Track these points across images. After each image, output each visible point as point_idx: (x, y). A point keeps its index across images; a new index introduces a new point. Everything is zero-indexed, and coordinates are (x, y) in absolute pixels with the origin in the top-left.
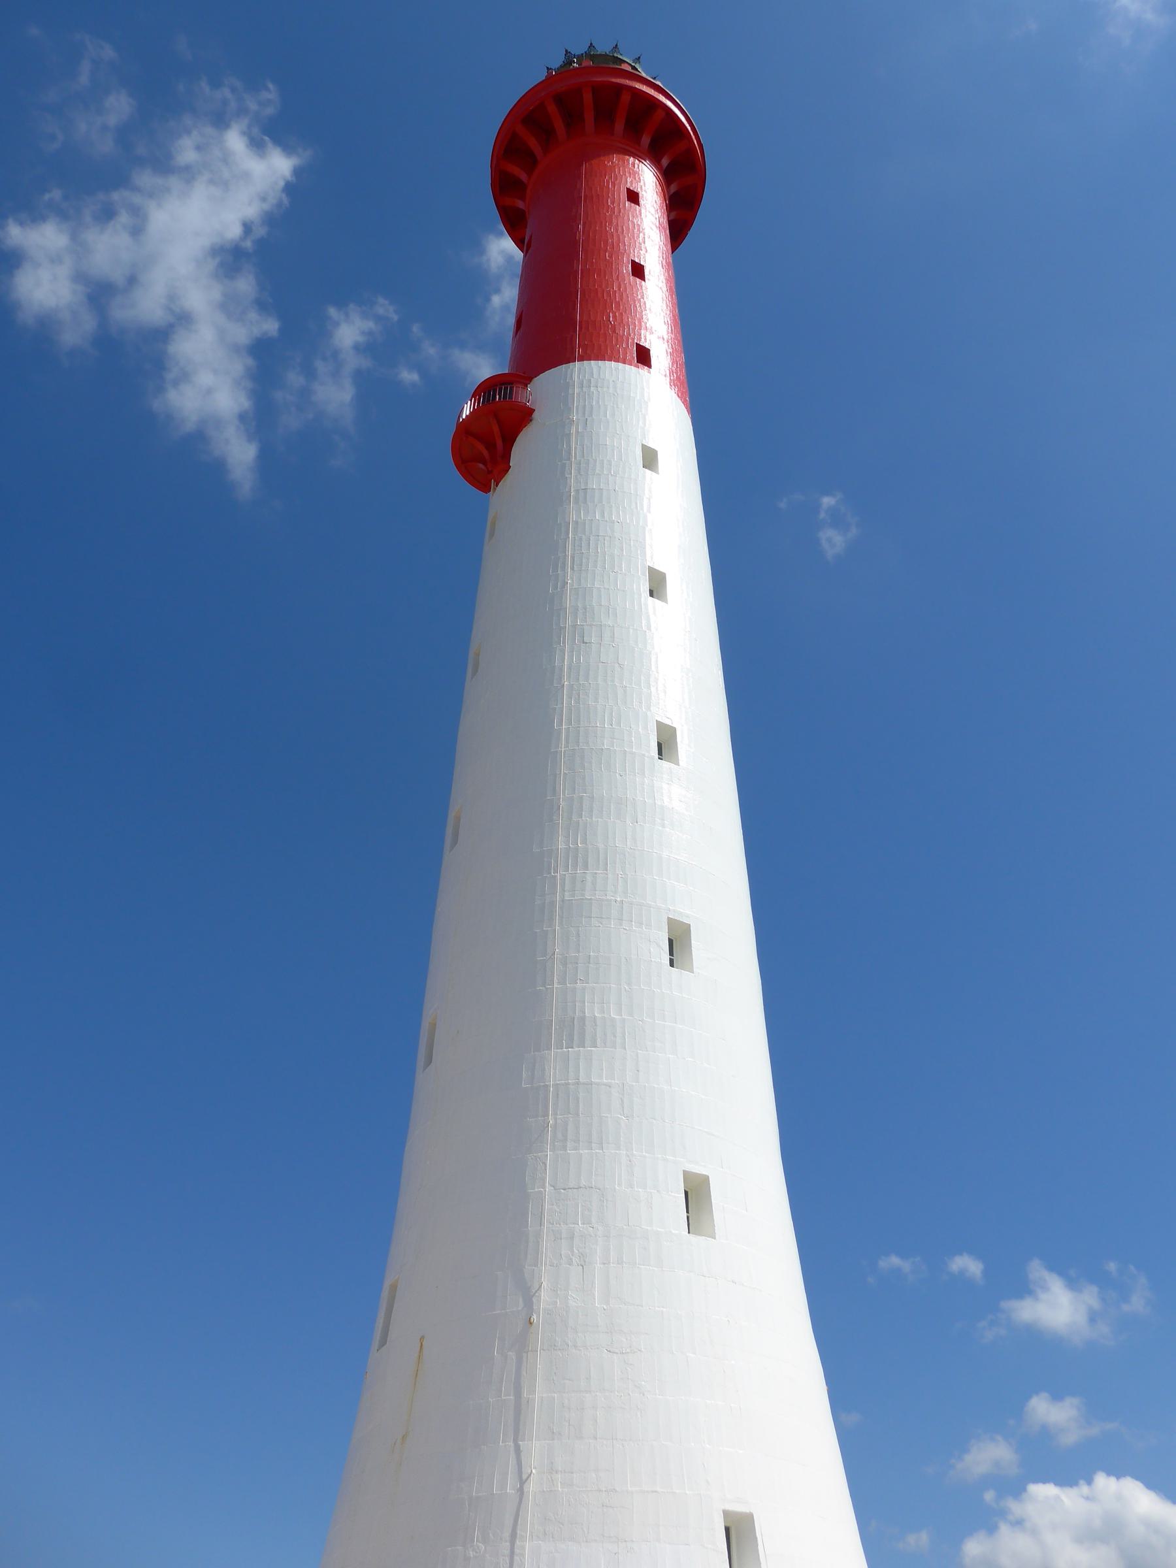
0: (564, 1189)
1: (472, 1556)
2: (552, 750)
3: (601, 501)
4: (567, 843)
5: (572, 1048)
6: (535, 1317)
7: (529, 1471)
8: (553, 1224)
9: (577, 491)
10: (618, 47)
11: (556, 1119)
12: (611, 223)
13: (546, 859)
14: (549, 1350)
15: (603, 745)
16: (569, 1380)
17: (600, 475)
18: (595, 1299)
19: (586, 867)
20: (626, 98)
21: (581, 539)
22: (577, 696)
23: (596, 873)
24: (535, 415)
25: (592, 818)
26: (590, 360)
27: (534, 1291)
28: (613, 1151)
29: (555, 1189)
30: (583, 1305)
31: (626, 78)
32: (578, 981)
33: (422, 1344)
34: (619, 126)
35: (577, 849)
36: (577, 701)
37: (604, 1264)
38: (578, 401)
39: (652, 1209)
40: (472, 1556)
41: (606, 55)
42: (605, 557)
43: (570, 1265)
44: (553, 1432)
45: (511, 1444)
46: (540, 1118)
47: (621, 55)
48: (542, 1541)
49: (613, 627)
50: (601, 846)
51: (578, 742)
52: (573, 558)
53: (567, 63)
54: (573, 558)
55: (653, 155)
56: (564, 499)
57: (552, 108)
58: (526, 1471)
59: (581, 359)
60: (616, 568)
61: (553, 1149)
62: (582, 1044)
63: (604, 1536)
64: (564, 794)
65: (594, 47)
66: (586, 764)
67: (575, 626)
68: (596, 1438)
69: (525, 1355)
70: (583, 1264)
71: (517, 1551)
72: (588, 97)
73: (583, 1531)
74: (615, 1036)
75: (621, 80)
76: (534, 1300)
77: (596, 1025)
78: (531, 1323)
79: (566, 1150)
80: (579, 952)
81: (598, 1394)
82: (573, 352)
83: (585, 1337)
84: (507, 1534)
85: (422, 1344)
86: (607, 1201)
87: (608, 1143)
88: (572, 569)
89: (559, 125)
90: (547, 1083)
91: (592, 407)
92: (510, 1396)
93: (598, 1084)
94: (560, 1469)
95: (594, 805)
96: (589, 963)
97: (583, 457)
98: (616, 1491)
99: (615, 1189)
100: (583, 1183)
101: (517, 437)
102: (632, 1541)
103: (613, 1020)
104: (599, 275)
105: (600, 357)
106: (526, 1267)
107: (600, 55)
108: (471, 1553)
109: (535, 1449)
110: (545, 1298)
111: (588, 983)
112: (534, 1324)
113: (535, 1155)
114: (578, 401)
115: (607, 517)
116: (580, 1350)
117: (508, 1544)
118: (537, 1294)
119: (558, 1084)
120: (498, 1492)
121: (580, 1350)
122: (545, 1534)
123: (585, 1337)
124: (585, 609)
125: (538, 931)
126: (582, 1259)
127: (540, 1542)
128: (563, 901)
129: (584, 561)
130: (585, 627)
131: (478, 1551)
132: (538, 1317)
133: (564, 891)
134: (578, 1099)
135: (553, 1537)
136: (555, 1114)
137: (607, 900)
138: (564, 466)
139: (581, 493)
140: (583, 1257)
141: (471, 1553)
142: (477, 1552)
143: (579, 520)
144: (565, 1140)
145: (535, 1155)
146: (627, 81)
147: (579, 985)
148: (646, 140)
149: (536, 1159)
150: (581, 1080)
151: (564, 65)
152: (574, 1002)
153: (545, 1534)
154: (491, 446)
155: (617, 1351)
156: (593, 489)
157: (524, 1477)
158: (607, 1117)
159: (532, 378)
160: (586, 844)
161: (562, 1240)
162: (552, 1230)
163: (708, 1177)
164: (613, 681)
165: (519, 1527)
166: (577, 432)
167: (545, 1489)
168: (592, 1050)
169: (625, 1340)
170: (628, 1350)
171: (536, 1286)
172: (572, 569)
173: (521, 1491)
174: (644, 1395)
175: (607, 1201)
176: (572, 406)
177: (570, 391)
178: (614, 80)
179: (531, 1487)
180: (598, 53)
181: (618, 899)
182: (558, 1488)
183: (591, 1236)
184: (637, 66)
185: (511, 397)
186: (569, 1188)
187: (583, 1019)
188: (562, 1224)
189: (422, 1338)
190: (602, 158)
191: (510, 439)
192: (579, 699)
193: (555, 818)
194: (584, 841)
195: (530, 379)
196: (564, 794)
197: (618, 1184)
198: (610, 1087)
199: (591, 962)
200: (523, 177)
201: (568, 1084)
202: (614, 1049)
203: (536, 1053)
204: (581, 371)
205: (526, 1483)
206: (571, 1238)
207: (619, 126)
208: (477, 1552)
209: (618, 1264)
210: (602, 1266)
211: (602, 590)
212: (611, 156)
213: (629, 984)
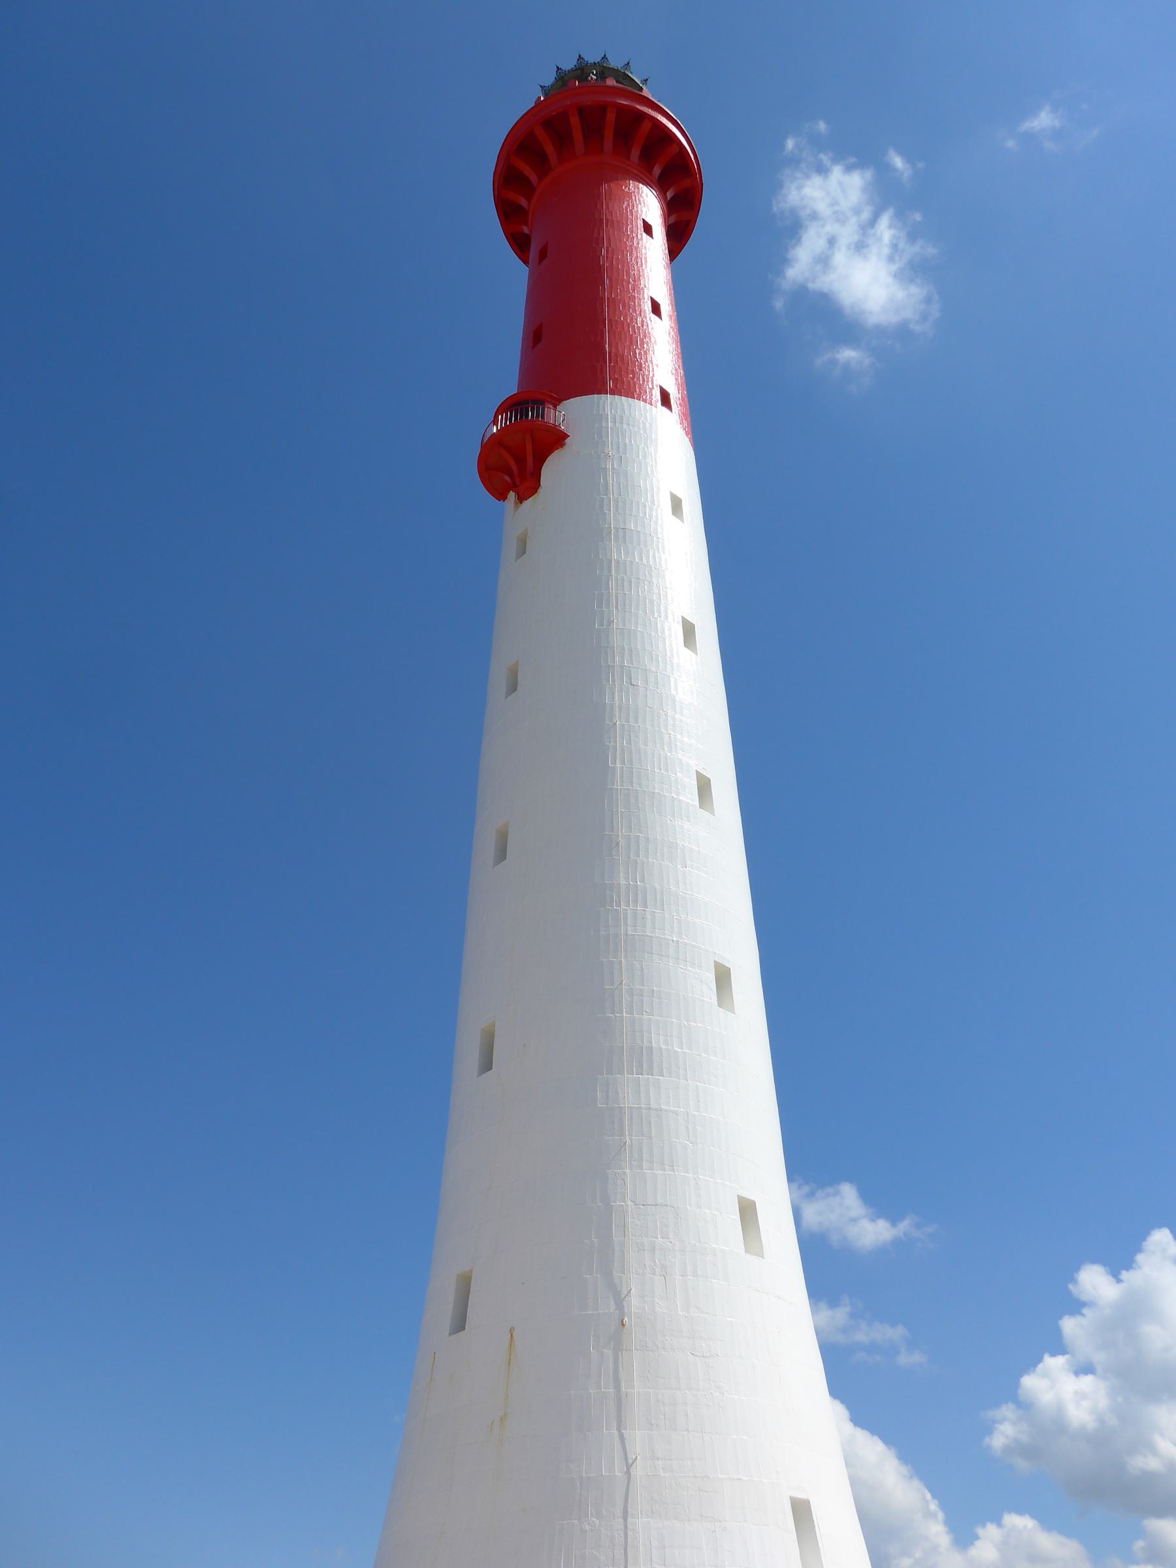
0: (643, 1205)
1: (588, 1529)
2: (609, 787)
3: (639, 544)
4: (627, 879)
5: (642, 1075)
6: (626, 1319)
7: (634, 1457)
8: (636, 1236)
9: (617, 529)
10: (630, 64)
11: (631, 1140)
12: (631, 254)
13: (608, 893)
14: (641, 1350)
15: (654, 788)
16: (662, 1378)
17: (636, 516)
18: (677, 1306)
19: (645, 905)
20: (646, 126)
21: (623, 580)
22: (628, 737)
23: (654, 912)
24: (567, 441)
25: (648, 859)
26: (601, 394)
27: (623, 1296)
28: (683, 1174)
29: (635, 1205)
30: (668, 1312)
31: (646, 106)
32: (644, 1013)
33: (512, 1335)
34: (635, 154)
35: (636, 887)
36: (629, 742)
37: (682, 1276)
38: (612, 436)
39: (717, 1228)
40: (588, 1529)
41: (618, 70)
42: (646, 601)
43: (654, 1274)
44: (651, 1424)
45: (615, 1432)
46: (616, 1137)
47: (631, 73)
48: (651, 1518)
49: (657, 673)
50: (657, 886)
51: (631, 782)
52: (617, 597)
53: (579, 69)
54: (617, 597)
55: (661, 186)
56: (604, 535)
57: (575, 120)
58: (631, 1457)
59: (613, 393)
60: (656, 614)
61: (631, 1168)
62: (621, 1072)
63: (702, 1516)
64: (622, 832)
65: (607, 59)
66: (640, 805)
67: (622, 667)
68: (688, 1430)
69: (620, 1353)
70: (665, 1274)
71: (629, 1526)
72: (611, 117)
73: (685, 1511)
74: (678, 1068)
75: (645, 108)
76: (625, 1303)
77: (662, 1056)
78: (623, 1325)
79: (642, 1169)
80: (643, 985)
81: (687, 1391)
82: (604, 383)
83: (672, 1340)
84: (619, 1511)
85: (512, 1335)
86: (681, 1219)
87: (678, 1166)
88: (617, 608)
89: (578, 136)
90: (622, 1106)
91: (625, 444)
92: (609, 1389)
93: (666, 1111)
94: (660, 1456)
95: (650, 847)
96: (653, 997)
97: (621, 496)
98: (709, 1478)
99: (687, 1209)
100: (660, 1201)
101: (547, 457)
102: (726, 1521)
103: (676, 1052)
104: (624, 306)
105: (602, 390)
106: (614, 1273)
107: (613, 69)
108: (587, 1526)
109: (637, 1438)
110: (634, 1303)
111: (653, 1016)
112: (625, 1326)
113: (615, 1171)
114: (612, 436)
115: (645, 561)
116: (668, 1352)
117: (621, 1520)
118: (626, 1299)
119: (631, 1107)
120: (607, 1474)
121: (668, 1352)
122: (653, 1513)
123: (672, 1340)
124: (631, 650)
125: (604, 960)
126: (663, 1270)
127: (649, 1520)
128: (626, 935)
129: (627, 602)
130: (633, 670)
131: (593, 1525)
132: (630, 1319)
133: (627, 925)
134: (650, 1123)
135: (660, 1516)
136: (631, 1135)
137: (666, 939)
138: (602, 501)
139: (621, 533)
140: (664, 1268)
141: (587, 1526)
142: (592, 1526)
143: (620, 560)
144: (641, 1160)
145: (615, 1171)
146: (650, 111)
147: (645, 1017)
148: (657, 171)
149: (615, 1175)
150: (652, 1106)
151: (576, 70)
152: (642, 1031)
153: (653, 1513)
154: (520, 460)
155: (698, 1354)
156: (631, 530)
157: (630, 1462)
158: (676, 1142)
159: (563, 400)
160: (644, 883)
161: (645, 1252)
162: (636, 1242)
163: (755, 1203)
164: (659, 727)
165: (629, 1506)
166: (613, 468)
167: (649, 1474)
168: (659, 1079)
169: (704, 1345)
170: (708, 1354)
171: (625, 1292)
172: (617, 608)
173: (628, 1473)
174: (723, 1394)
175: (681, 1219)
176: (606, 440)
177: (604, 424)
178: (638, 107)
179: (638, 1471)
180: (611, 66)
181: (675, 939)
182: (660, 1472)
183: (669, 1250)
184: (644, 87)
185: (543, 418)
186: (648, 1205)
187: (650, 1049)
188: (643, 1236)
189: (512, 1330)
190: (620, 182)
191: (540, 460)
192: (630, 740)
193: (614, 853)
194: (643, 880)
195: (560, 401)
196: (622, 832)
197: (689, 1204)
198: (677, 1114)
199: (655, 996)
200: (533, 178)
201: (641, 1108)
202: (677, 1080)
203: (609, 1076)
204: (610, 403)
205: (632, 1467)
206: (653, 1250)
207: (608, 145)
208: (592, 1526)
209: (694, 1276)
210: (681, 1278)
211: (645, 634)
212: (627, 181)
213: (688, 1021)
